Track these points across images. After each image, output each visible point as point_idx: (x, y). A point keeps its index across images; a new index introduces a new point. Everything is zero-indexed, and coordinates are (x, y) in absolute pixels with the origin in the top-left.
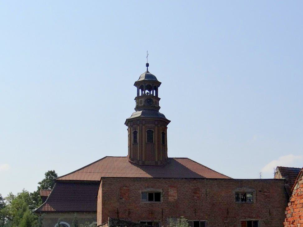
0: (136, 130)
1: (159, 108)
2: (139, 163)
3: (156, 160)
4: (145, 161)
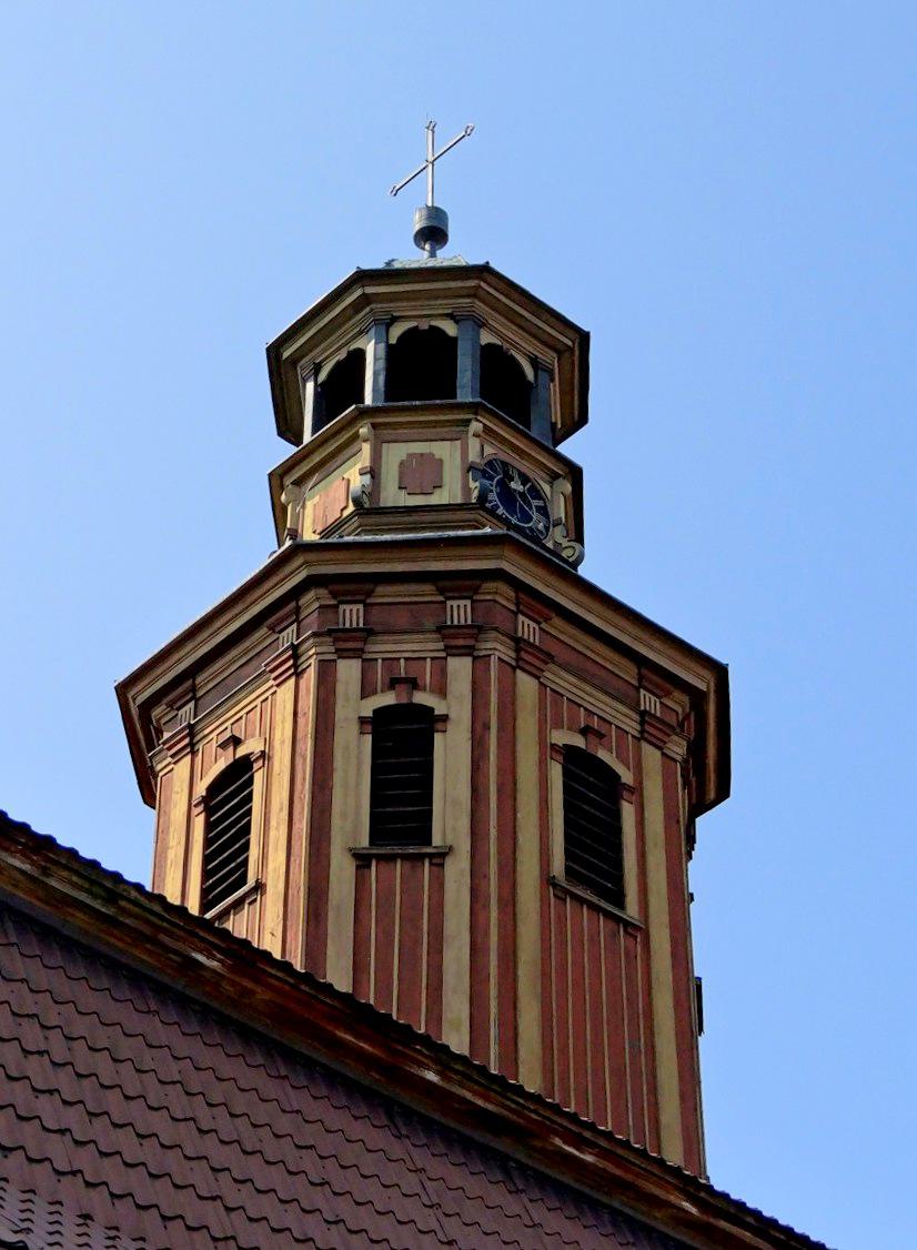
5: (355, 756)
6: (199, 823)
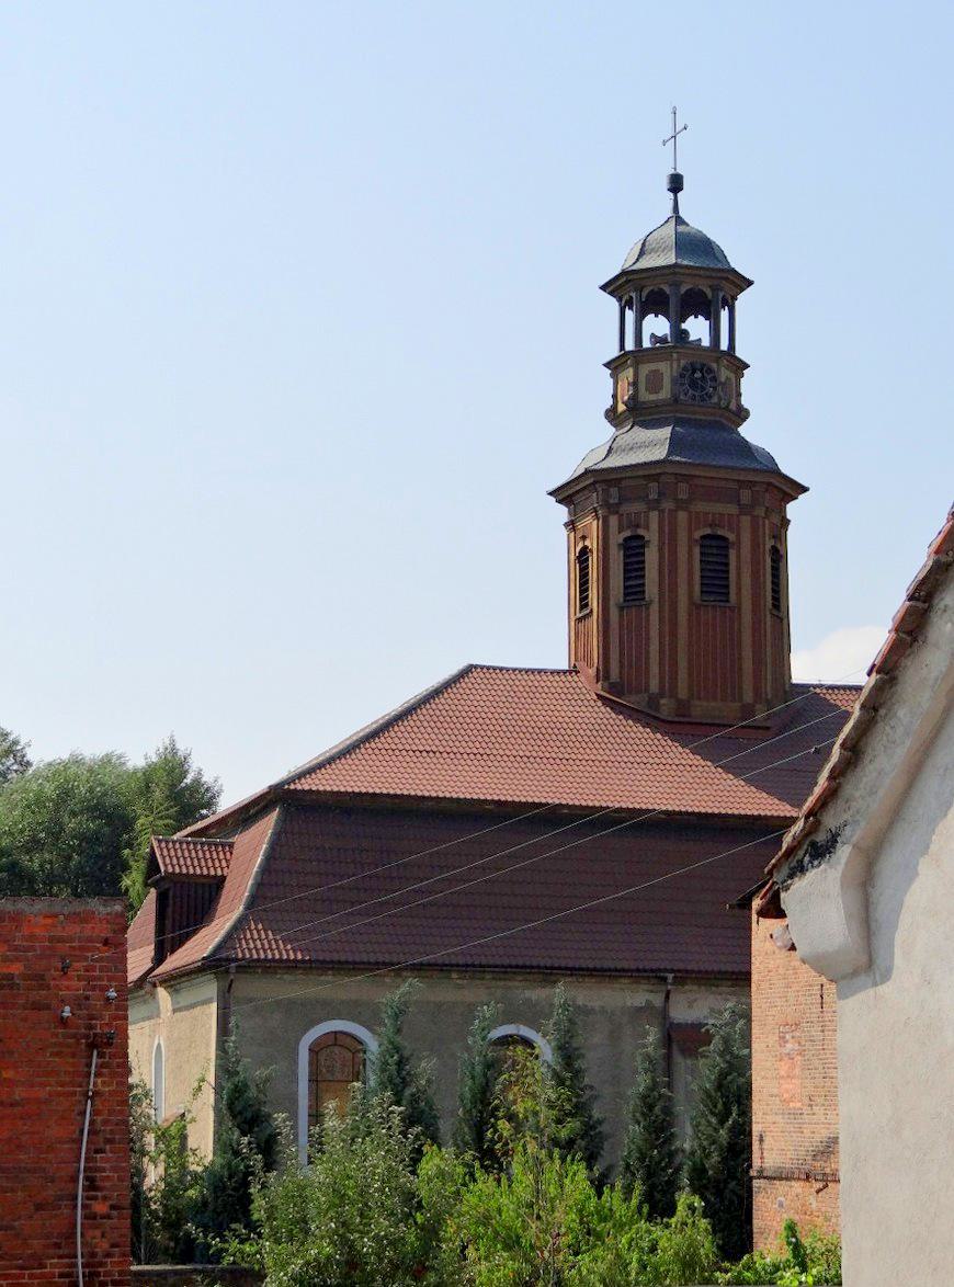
0: (641, 532)
1: (742, 415)
2: (657, 708)
3: (748, 697)
4: (756, 702)
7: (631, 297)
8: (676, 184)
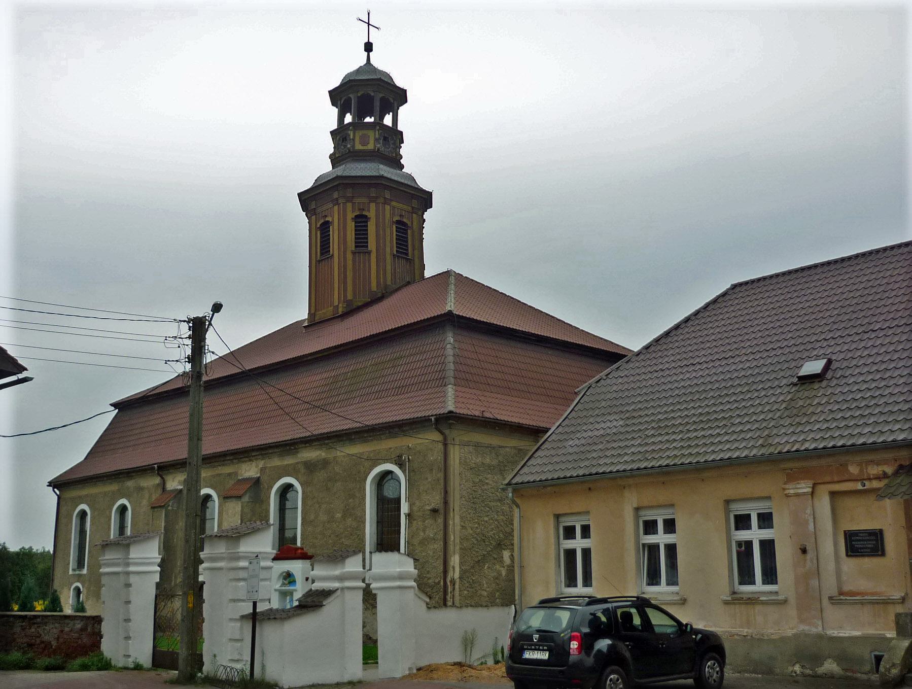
0: (364, 213)
5: (351, 226)
6: (319, 233)
7: (350, 98)
8: (369, 47)
